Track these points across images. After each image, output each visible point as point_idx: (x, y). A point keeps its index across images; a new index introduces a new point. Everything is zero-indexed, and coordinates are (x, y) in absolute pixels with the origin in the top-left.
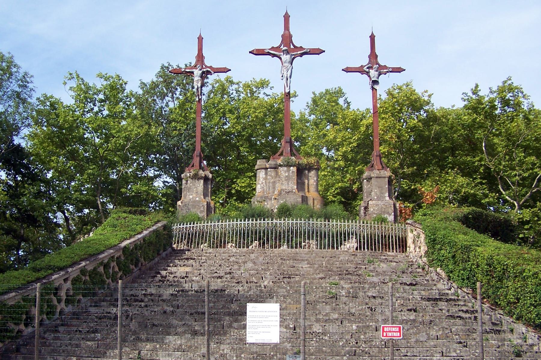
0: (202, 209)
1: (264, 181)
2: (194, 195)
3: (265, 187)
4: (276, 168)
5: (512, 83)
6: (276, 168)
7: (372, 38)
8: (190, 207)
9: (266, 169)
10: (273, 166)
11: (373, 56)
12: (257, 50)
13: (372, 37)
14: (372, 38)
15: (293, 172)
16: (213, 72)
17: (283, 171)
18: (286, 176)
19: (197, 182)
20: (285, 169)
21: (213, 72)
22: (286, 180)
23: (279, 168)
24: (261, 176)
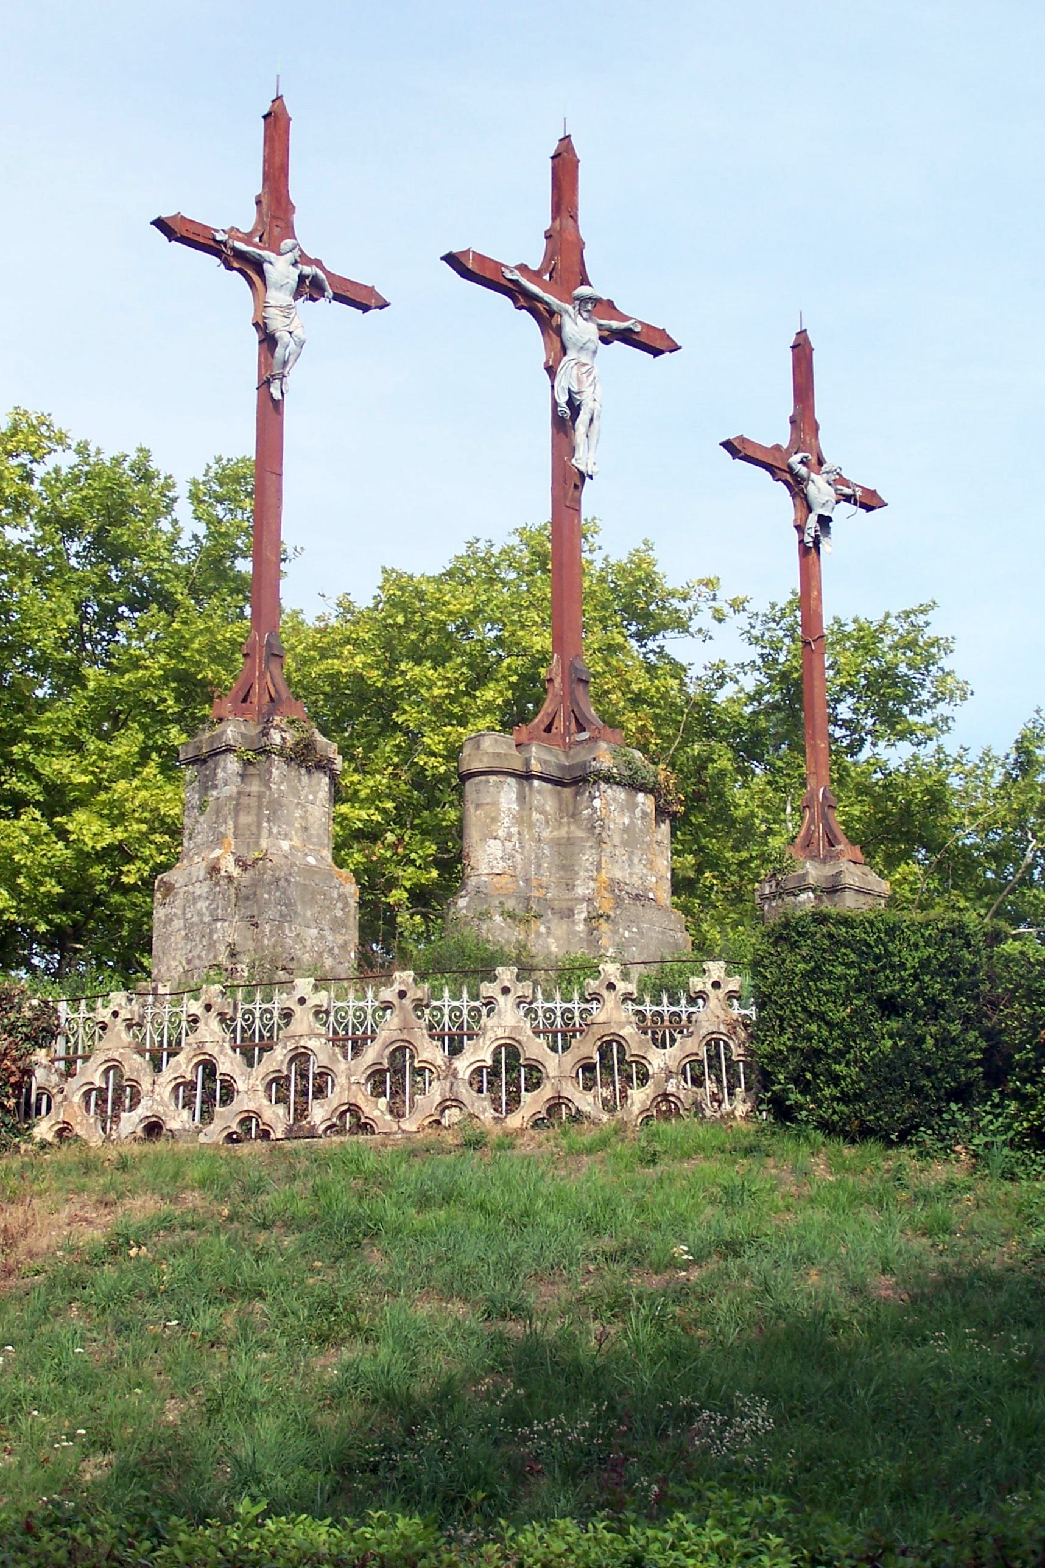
0: (339, 913)
1: (514, 830)
2: (296, 842)
3: (518, 857)
4: (576, 780)
5: (855, 621)
6: (576, 780)
7: (802, 351)
8: (294, 893)
9: (526, 777)
10: (554, 773)
11: (804, 420)
12: (480, 258)
13: (802, 352)
14: (802, 351)
15: (645, 814)
16: (330, 293)
17: (608, 801)
18: (626, 830)
19: (305, 779)
20: (621, 794)
21: (330, 293)
22: (625, 844)
23: (603, 786)
24: (504, 806)
